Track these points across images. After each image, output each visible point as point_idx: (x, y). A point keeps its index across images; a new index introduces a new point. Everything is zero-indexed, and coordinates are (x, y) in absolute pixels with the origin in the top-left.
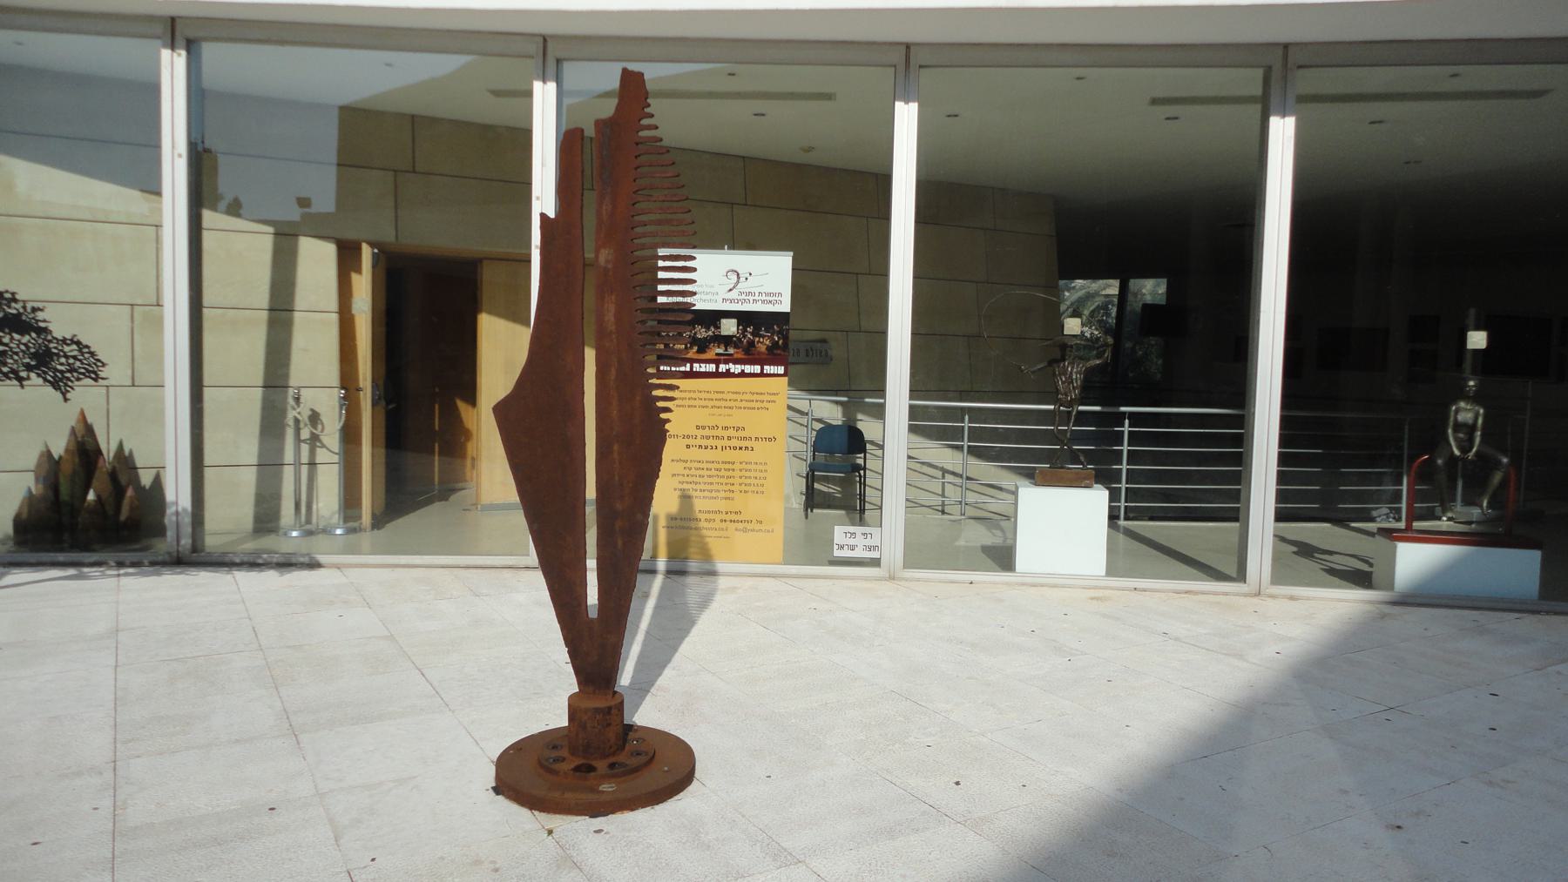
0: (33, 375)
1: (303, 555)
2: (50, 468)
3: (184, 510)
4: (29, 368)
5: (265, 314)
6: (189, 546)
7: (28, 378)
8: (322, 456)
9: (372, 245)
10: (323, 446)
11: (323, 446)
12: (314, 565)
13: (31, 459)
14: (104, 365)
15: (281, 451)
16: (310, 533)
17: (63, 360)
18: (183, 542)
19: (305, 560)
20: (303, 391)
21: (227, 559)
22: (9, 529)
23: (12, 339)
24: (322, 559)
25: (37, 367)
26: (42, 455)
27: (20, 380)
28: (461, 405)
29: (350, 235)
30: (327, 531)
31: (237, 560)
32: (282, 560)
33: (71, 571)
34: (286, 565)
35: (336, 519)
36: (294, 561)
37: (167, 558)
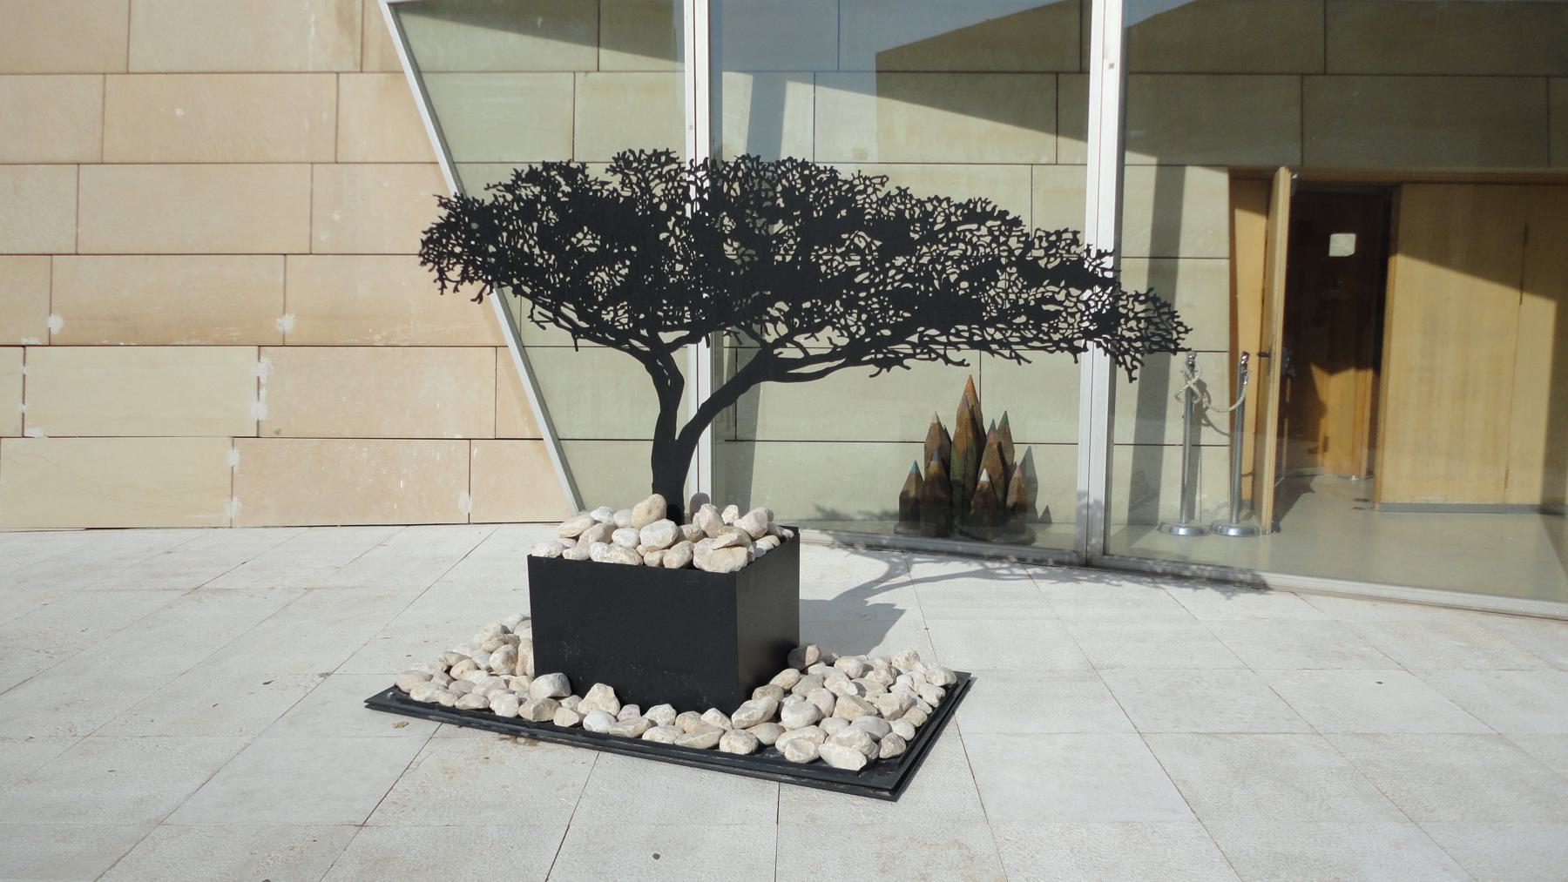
0: (1090, 344)
1: (1242, 571)
2: (940, 443)
3: (1097, 502)
4: (1088, 335)
5: (1145, 263)
6: (1100, 547)
7: (1085, 349)
8: (1207, 435)
9: (1292, 170)
10: (1209, 424)
11: (1209, 424)
12: (1260, 586)
13: (922, 432)
14: (1187, 331)
15: (1161, 430)
16: (1199, 532)
17: (1133, 324)
18: (1094, 541)
19: (1248, 577)
20: (1199, 358)
21: (1145, 567)
22: (894, 506)
23: (1068, 295)
24: (1270, 578)
25: (1097, 333)
26: (933, 427)
27: (1075, 351)
28: (1317, 372)
29: (1249, 159)
30: (1216, 529)
31: (1159, 570)
32: (1215, 574)
33: (975, 566)
34: (1223, 581)
35: (1224, 513)
36: (1231, 577)
37: (1074, 558)
